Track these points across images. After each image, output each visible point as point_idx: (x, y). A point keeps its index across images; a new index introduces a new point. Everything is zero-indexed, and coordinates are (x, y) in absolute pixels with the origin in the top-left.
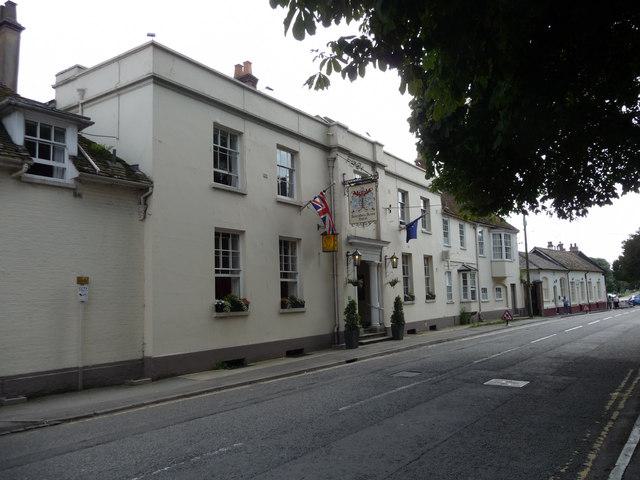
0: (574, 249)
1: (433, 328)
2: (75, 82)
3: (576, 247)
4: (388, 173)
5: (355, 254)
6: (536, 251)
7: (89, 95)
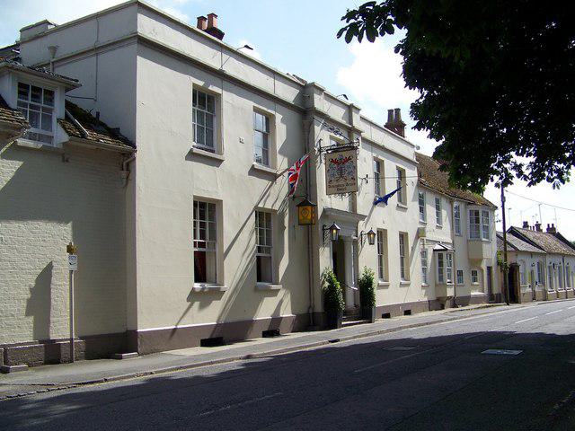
0: (551, 230)
1: (408, 313)
2: (43, 39)
3: (553, 229)
4: (365, 140)
5: (332, 228)
6: (513, 231)
7: (62, 53)
